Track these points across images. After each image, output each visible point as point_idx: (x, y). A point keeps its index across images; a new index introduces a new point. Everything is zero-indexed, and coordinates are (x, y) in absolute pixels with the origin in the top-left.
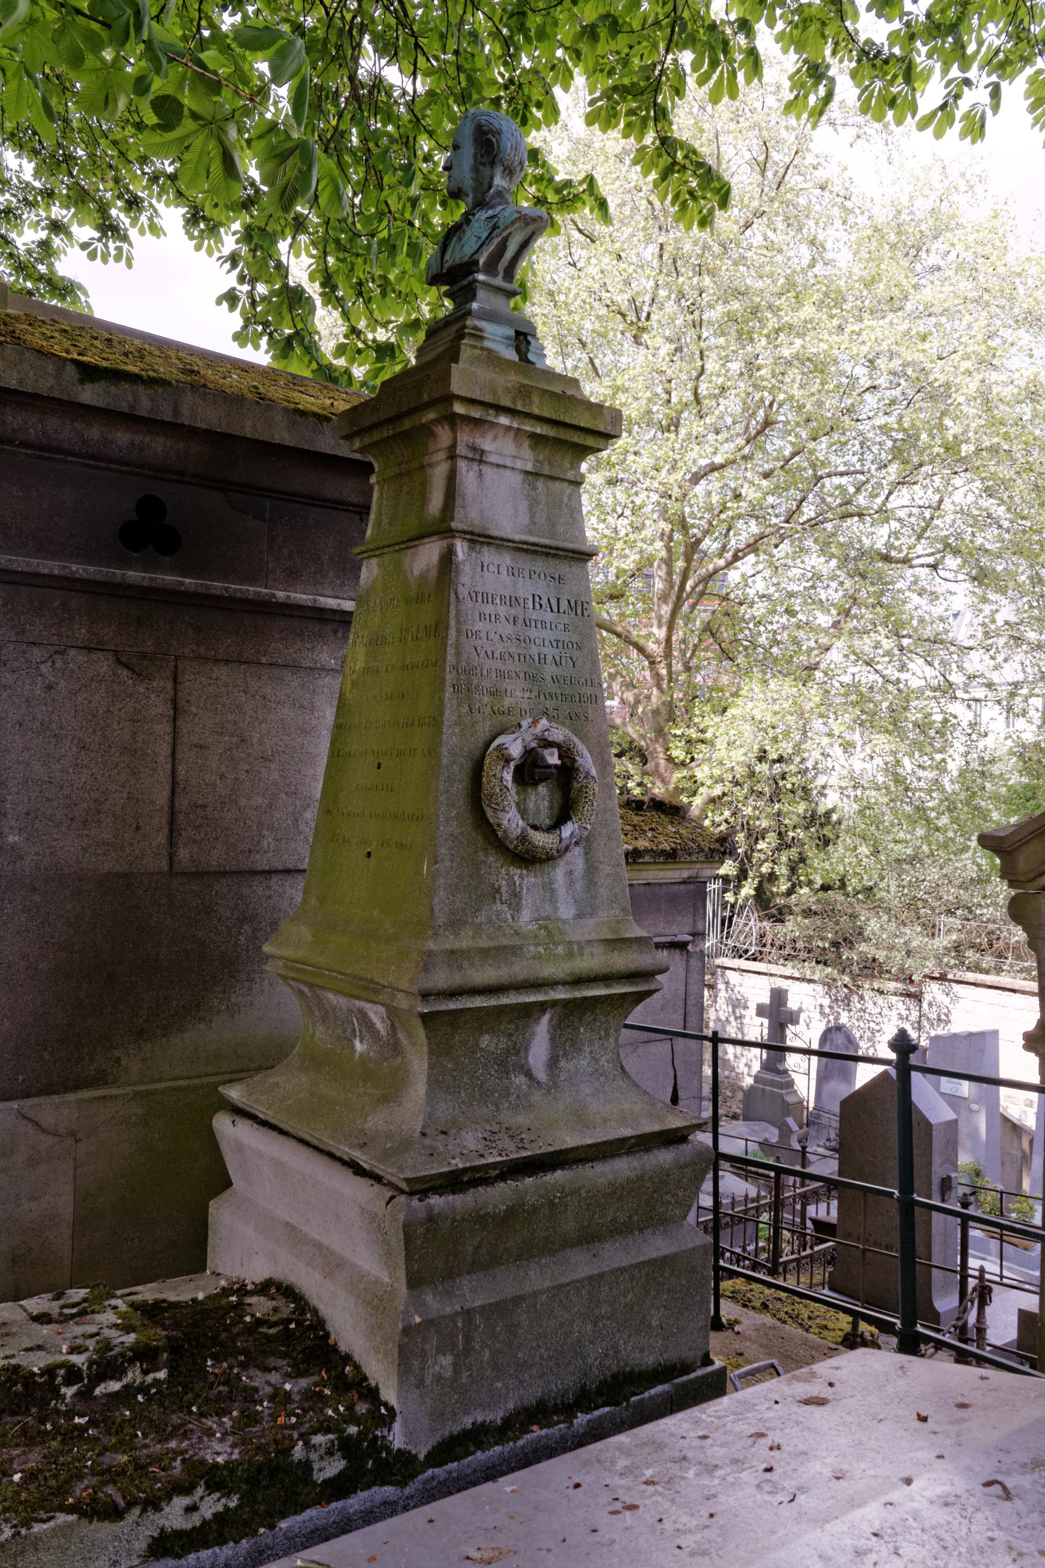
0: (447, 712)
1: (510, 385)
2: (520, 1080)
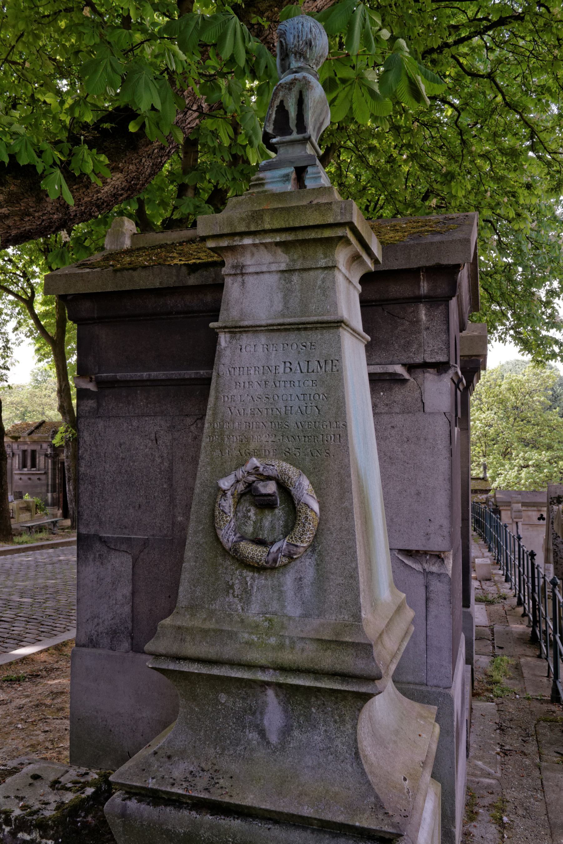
0: (202, 456)
1: (244, 216)
2: (253, 736)
